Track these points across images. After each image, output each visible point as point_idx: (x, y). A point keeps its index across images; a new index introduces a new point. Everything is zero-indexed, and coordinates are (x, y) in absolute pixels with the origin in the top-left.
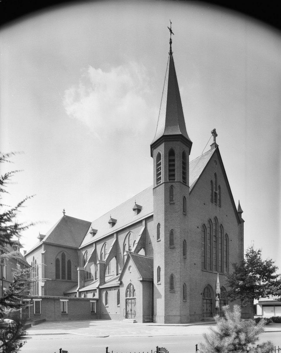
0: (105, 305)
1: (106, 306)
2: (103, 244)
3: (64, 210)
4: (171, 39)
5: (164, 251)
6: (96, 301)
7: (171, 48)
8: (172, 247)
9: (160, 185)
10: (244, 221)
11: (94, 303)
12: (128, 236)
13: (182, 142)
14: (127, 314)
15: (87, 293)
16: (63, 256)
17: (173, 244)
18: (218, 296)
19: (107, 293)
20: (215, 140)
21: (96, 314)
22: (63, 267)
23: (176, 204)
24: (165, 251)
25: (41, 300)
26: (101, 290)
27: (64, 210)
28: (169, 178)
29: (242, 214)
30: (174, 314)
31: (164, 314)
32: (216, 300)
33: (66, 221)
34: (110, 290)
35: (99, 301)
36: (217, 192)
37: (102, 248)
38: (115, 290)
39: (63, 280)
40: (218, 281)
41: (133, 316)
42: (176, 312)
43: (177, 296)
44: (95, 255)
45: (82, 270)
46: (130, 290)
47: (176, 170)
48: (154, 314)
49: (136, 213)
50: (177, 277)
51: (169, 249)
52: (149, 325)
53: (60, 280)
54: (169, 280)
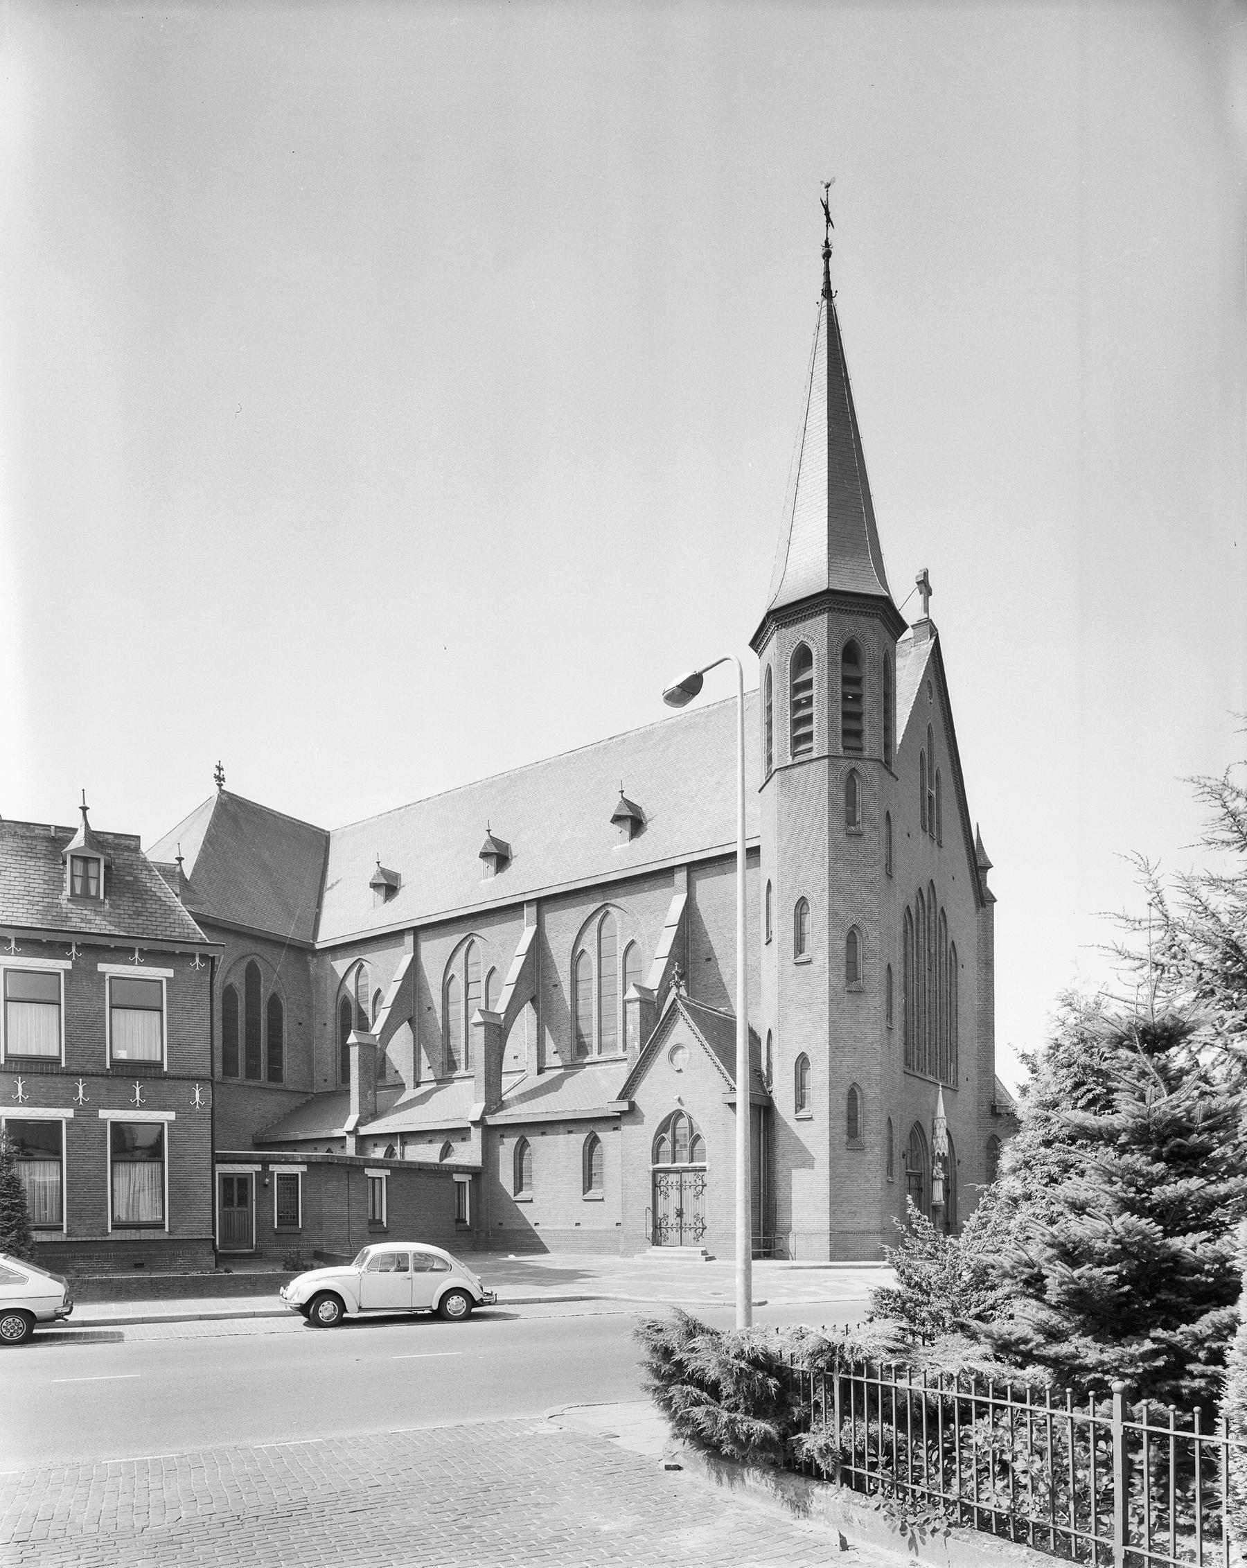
0: (510, 1189)
1: (518, 1198)
2: (457, 938)
3: (220, 769)
4: (827, 244)
5: (827, 999)
6: (470, 1177)
7: (827, 273)
8: (853, 986)
9: (811, 761)
10: (995, 901)
11: (464, 1183)
12: (599, 917)
13: (882, 620)
14: (656, 1227)
15: (404, 1144)
16: (252, 975)
17: (856, 979)
18: (940, 1165)
19: (522, 1146)
20: (926, 610)
21: (469, 1230)
22: (253, 1024)
23: (866, 836)
24: (831, 1000)
25: (304, 1168)
26: (492, 1134)
27: (220, 769)
28: (843, 742)
29: (990, 873)
30: (862, 1227)
31: (826, 1227)
32: (934, 1179)
33: (235, 819)
34: (543, 1134)
35: (482, 1175)
36: (934, 793)
37: (453, 955)
38: (570, 1132)
39: (251, 1083)
40: (941, 1111)
41: (690, 1235)
42: (867, 1220)
43: (870, 1163)
44: (415, 986)
45: (368, 1045)
46: (674, 1135)
47: (866, 718)
48: (780, 1225)
49: (627, 834)
50: (872, 1094)
51: (846, 995)
52: (792, 1268)
53: (240, 1082)
54: (843, 1106)
